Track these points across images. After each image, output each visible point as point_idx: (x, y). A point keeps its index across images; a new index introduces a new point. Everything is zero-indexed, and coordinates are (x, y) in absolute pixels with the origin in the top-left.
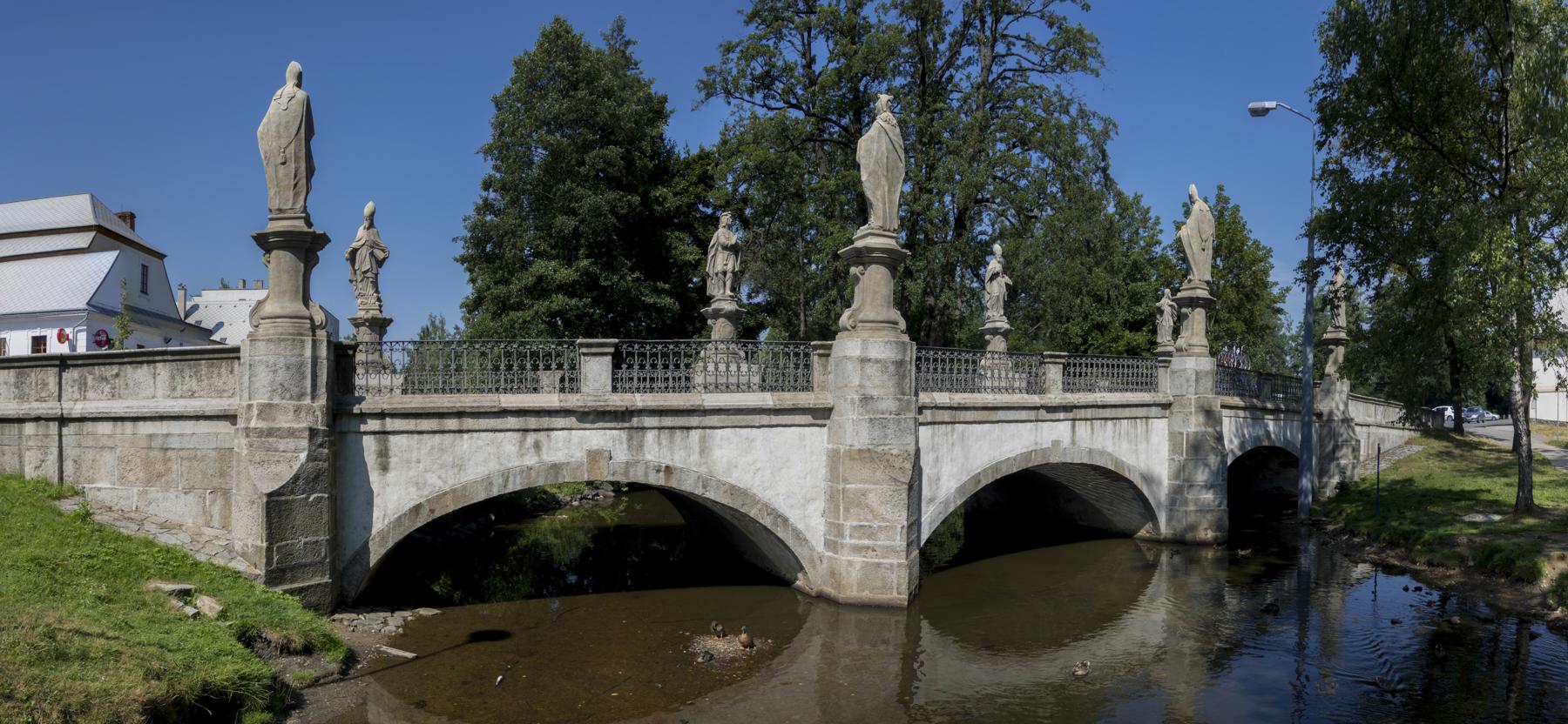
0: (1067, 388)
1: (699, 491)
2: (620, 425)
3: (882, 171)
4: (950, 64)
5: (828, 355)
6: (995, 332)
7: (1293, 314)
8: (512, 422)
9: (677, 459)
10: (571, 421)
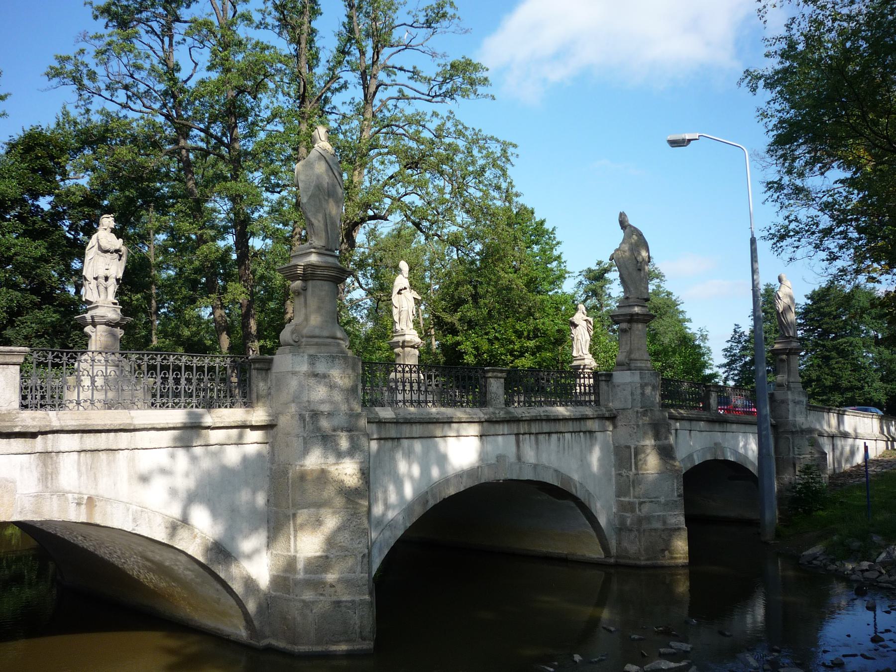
5: (268, 370)
9: (103, 488)
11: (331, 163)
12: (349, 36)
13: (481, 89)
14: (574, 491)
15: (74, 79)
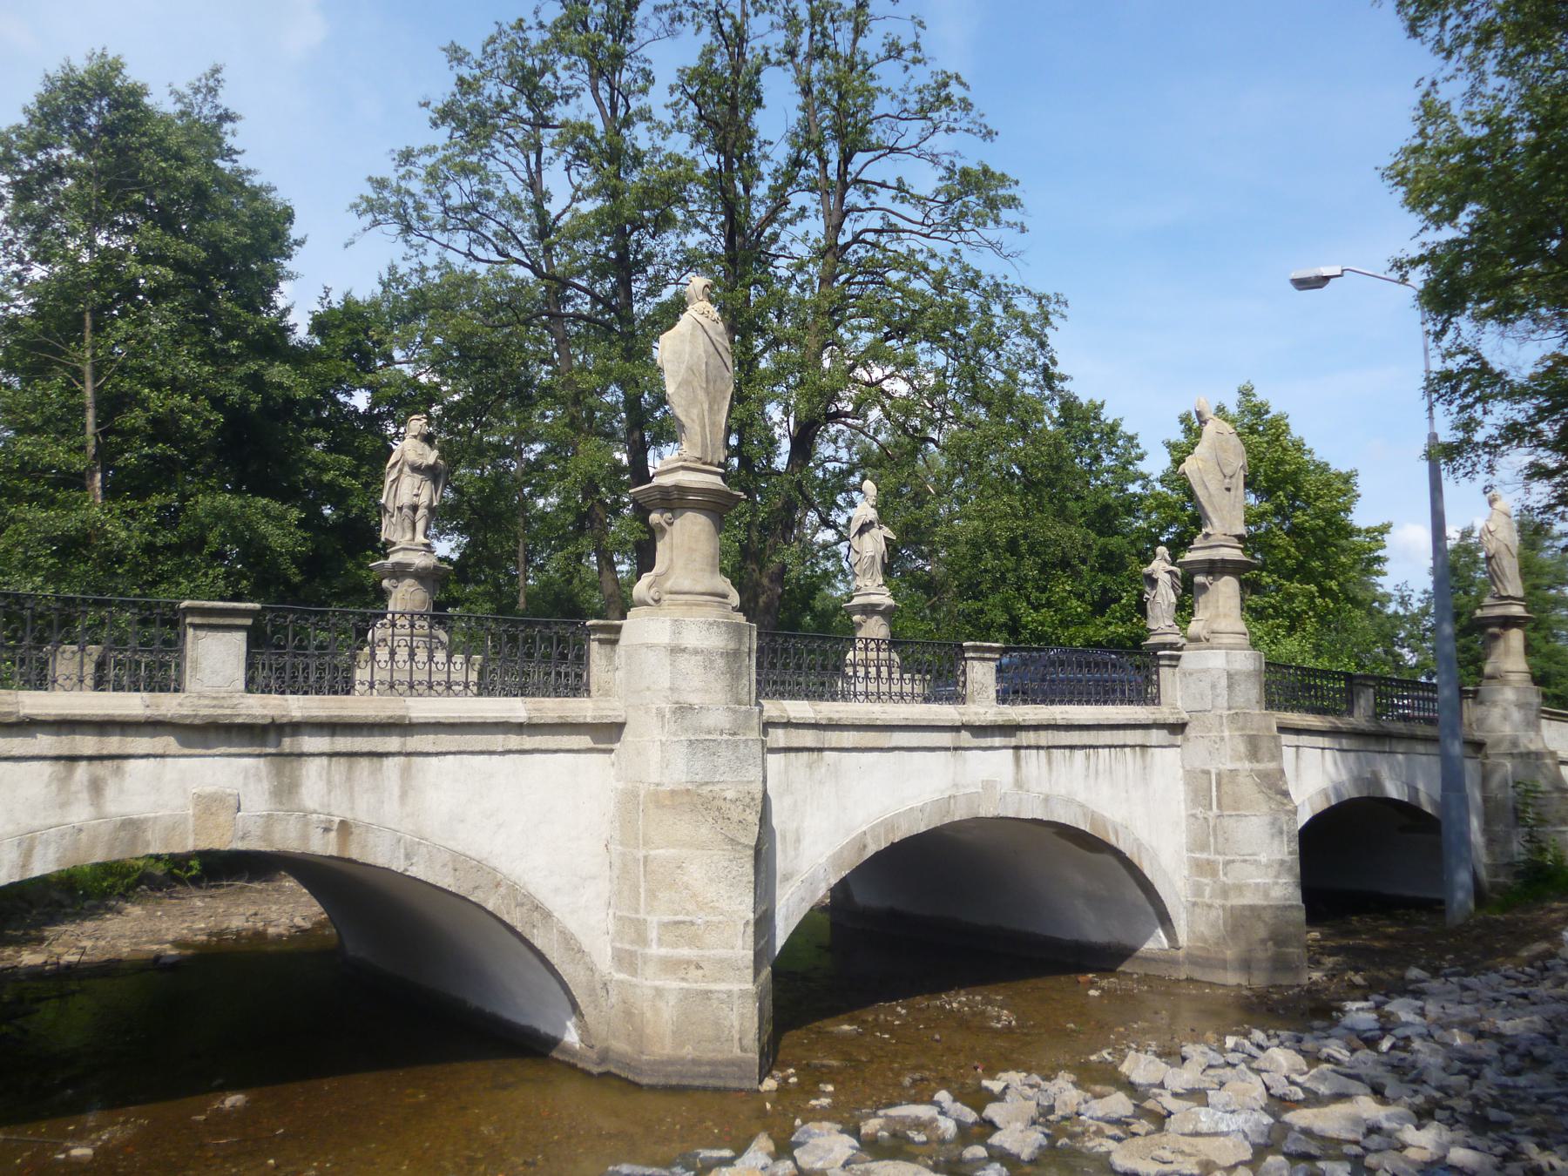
0: (1003, 698)
1: (398, 866)
2: (257, 750)
3: (699, 382)
4: (771, 218)
5: (615, 642)
6: (870, 610)
7: (1406, 572)
8: (44, 743)
9: (361, 810)
10: (168, 743)
11: (711, 333)
12: (807, 140)
13: (1006, 214)
14: (1113, 841)
15: (397, 215)
